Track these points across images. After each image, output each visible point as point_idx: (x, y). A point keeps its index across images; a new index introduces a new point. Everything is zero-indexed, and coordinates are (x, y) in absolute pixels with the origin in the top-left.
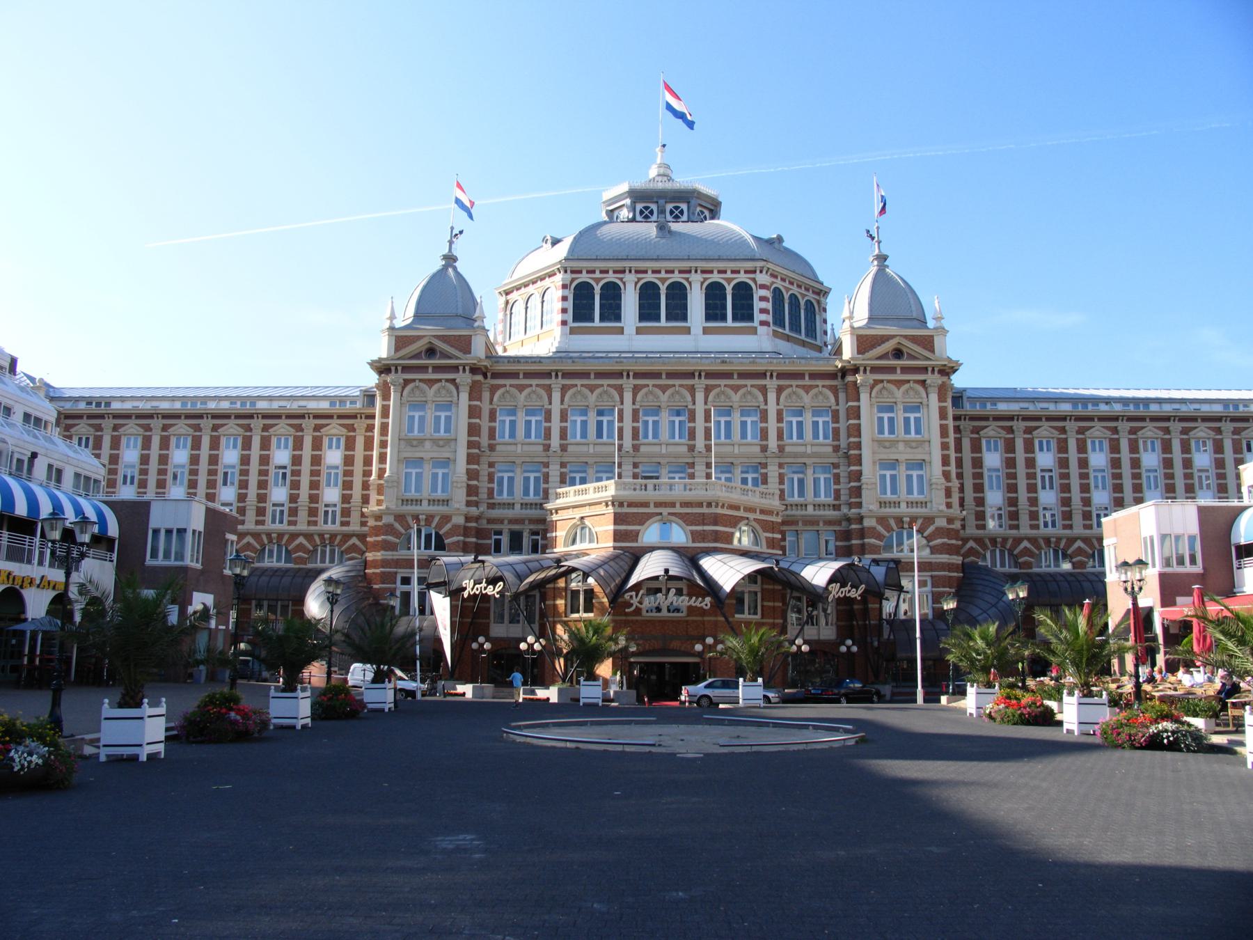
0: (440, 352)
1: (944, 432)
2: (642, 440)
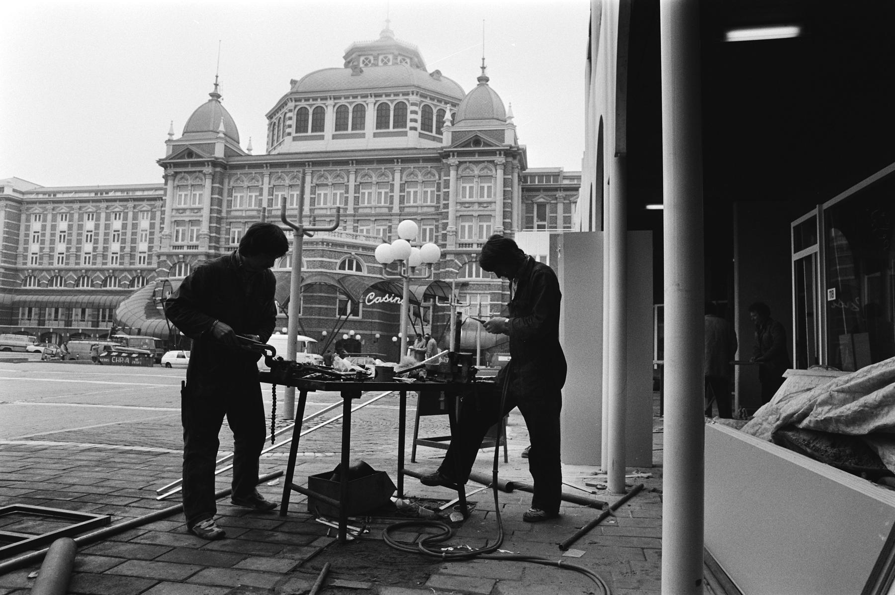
0: (484, 142)
2: (317, 206)
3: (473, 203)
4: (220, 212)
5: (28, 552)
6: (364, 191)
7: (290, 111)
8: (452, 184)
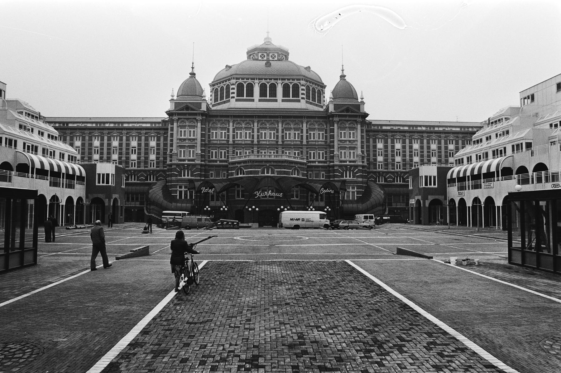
1: (362, 137)
3: (346, 141)
4: (204, 141)
5: (520, 223)
6: (262, 132)
7: (233, 84)
8: (336, 130)
